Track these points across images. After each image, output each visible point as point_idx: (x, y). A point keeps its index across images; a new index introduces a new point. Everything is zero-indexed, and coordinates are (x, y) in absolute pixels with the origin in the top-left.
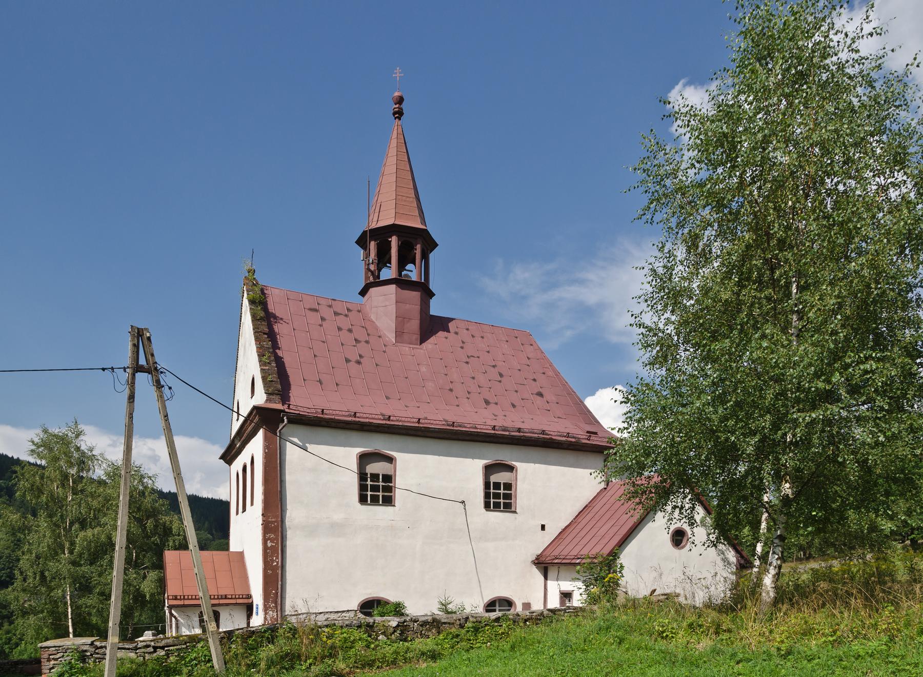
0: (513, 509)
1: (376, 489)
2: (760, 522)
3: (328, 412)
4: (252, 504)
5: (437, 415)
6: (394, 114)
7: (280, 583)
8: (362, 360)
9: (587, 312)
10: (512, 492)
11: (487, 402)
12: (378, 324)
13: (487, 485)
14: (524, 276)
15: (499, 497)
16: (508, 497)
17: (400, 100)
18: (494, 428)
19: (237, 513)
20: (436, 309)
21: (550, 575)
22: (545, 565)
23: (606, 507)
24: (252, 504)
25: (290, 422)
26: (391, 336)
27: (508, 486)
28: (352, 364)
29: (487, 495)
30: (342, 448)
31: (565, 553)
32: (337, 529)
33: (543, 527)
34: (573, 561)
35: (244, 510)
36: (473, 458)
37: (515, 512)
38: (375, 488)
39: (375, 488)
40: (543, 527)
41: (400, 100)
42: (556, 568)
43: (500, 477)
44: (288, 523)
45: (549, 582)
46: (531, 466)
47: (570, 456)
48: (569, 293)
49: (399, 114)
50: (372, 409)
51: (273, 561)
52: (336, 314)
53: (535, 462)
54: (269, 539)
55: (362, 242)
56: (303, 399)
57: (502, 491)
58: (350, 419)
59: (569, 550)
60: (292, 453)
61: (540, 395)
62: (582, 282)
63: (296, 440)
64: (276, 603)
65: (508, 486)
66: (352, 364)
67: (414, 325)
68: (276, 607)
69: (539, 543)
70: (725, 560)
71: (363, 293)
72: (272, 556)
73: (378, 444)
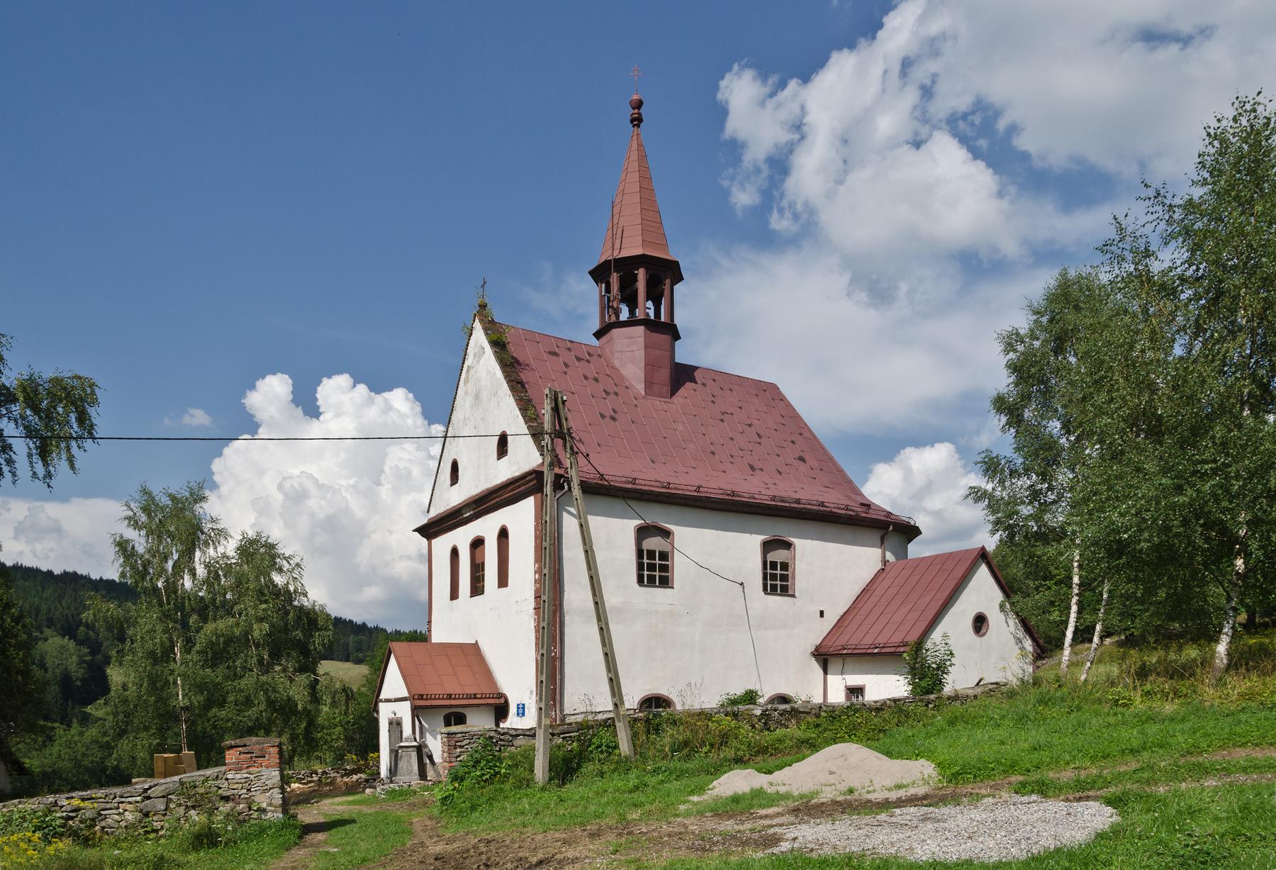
0: (790, 592)
1: (654, 569)
2: (1069, 608)
4: (503, 581)
5: (715, 483)
6: (632, 121)
7: (558, 677)
8: (616, 416)
11: (752, 468)
12: (624, 372)
15: (777, 579)
16: (784, 578)
17: (638, 105)
18: (773, 498)
19: (454, 595)
20: (684, 354)
22: (825, 657)
23: (892, 591)
24: (503, 581)
26: (640, 387)
27: (785, 566)
28: (607, 419)
29: (640, 567)
31: (854, 641)
33: (822, 613)
35: (477, 588)
36: (751, 533)
37: (793, 596)
38: (651, 567)
39: (651, 567)
40: (822, 613)
41: (638, 105)
42: (841, 660)
43: (778, 555)
44: (565, 607)
45: (829, 677)
47: (847, 532)
49: (637, 121)
50: (650, 475)
52: (579, 359)
55: (600, 274)
57: (779, 572)
58: (630, 486)
61: (802, 459)
65: (785, 566)
66: (607, 419)
67: (664, 374)
68: (555, 705)
69: (817, 632)
70: (1022, 649)
71: (598, 335)
73: (781, 529)
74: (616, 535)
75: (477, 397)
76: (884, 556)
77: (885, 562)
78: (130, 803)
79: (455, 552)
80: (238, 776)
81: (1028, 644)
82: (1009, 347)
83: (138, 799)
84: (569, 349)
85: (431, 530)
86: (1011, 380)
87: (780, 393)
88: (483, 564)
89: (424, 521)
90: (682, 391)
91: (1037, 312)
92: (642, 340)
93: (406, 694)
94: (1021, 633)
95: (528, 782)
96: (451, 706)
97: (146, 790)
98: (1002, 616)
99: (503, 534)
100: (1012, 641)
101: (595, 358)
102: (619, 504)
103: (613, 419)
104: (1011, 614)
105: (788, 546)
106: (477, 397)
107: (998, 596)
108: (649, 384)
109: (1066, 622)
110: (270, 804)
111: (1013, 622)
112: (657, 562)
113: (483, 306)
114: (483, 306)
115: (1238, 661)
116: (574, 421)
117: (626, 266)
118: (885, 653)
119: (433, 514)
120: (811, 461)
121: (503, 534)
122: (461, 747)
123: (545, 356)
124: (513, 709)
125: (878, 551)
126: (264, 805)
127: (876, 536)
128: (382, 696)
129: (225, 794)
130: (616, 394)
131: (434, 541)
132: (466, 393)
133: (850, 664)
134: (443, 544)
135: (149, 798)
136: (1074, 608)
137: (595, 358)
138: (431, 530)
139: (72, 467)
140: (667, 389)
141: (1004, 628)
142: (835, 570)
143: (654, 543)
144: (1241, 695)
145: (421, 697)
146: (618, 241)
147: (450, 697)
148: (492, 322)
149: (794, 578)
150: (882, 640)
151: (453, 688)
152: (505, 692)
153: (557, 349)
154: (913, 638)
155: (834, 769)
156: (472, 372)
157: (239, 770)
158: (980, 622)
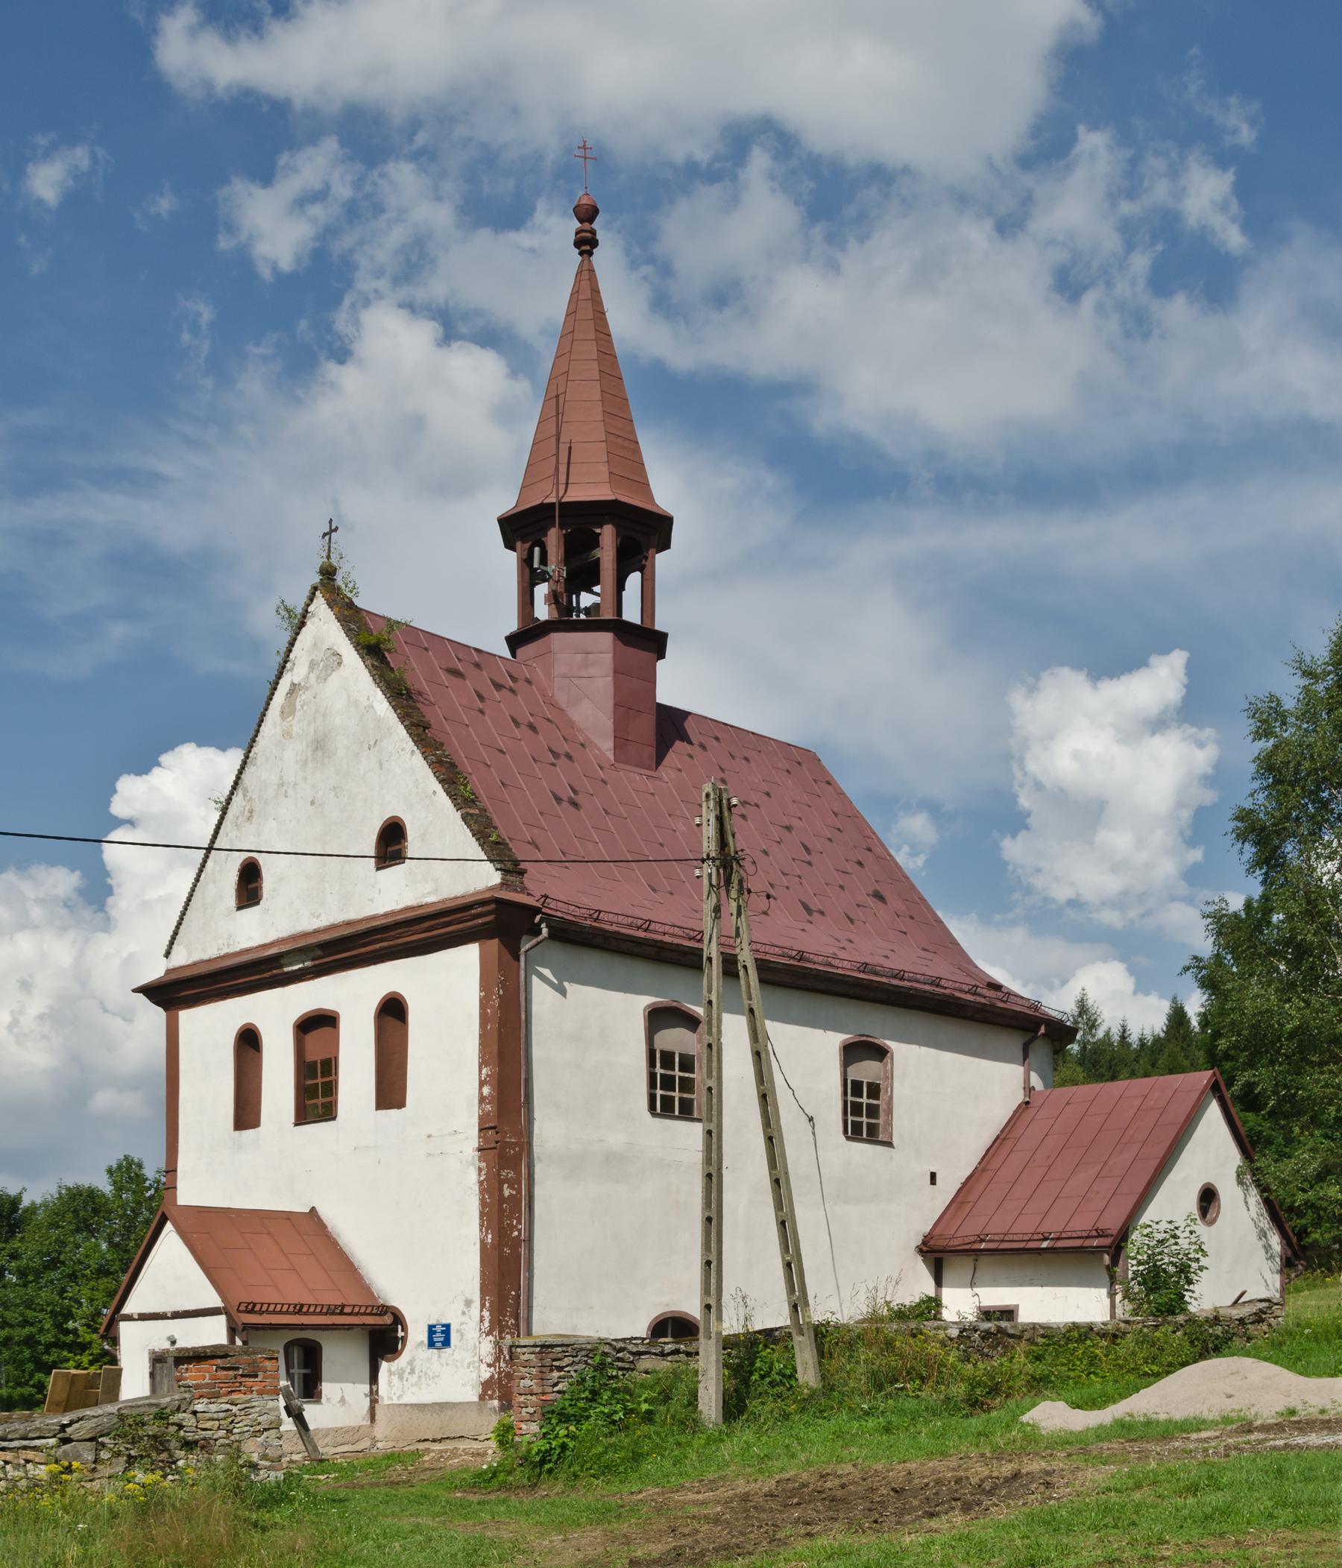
0: (881, 1137)
3: (657, 927)
4: (390, 1091)
8: (578, 799)
13: (651, 1053)
18: (865, 967)
20: (675, 684)
21: (947, 1275)
24: (390, 1091)
25: (552, 936)
26: (606, 746)
27: (874, 1091)
28: (565, 805)
30: (621, 995)
32: (615, 1164)
33: (933, 1177)
34: (976, 1246)
36: (825, 1029)
37: (889, 1144)
38: (668, 1083)
40: (933, 1177)
42: (970, 1259)
43: (866, 1070)
46: (914, 1048)
47: (948, 1028)
51: (512, 1228)
52: (498, 686)
53: (920, 1044)
54: (506, 1181)
57: (864, 1100)
58: (641, 934)
59: (968, 1230)
60: (542, 997)
61: (878, 896)
63: (546, 972)
64: (517, 1317)
67: (646, 726)
68: (517, 1325)
69: (924, 1211)
70: (1267, 1248)
72: (511, 1218)
73: (873, 1023)
74: (592, 1029)
75: (319, 745)
76: (1027, 1080)
77: (1029, 1089)
78: (35, 1448)
79: (248, 1041)
80: (213, 1408)
81: (1275, 1241)
82: (1263, 731)
83: (52, 1441)
84: (477, 665)
85: (174, 993)
87: (823, 769)
88: (336, 1059)
89: (155, 971)
90: (671, 757)
92: (608, 658)
94: (1265, 1223)
95: (689, 1421)
96: (303, 1327)
97: (63, 1427)
98: (1238, 1191)
99: (393, 1010)
100: (1254, 1232)
101: (522, 684)
102: (619, 966)
103: (574, 804)
104: (1254, 1191)
105: (880, 1053)
106: (319, 745)
107: (1232, 1156)
108: (621, 741)
111: (1254, 1197)
112: (677, 1073)
113: (328, 573)
114: (328, 573)
117: (581, 521)
119: (182, 957)
120: (894, 902)
121: (393, 1010)
122: (560, 1369)
123: (444, 677)
124: (416, 1334)
126: (255, 1457)
127: (1014, 1042)
128: (126, 1310)
129: (190, 1437)
130: (569, 757)
131: (186, 1017)
132: (287, 734)
134: (211, 1027)
135: (66, 1441)
137: (522, 684)
138: (174, 993)
140: (650, 751)
141: (1242, 1211)
142: (957, 1098)
145: (251, 1308)
146: (563, 469)
147: (299, 1309)
148: (351, 605)
149: (890, 1112)
150: (1053, 1225)
151: (297, 1294)
152: (394, 1301)
153: (461, 661)
155: (1230, 1392)
156: (303, 697)
157: (214, 1397)
158: (1208, 1197)
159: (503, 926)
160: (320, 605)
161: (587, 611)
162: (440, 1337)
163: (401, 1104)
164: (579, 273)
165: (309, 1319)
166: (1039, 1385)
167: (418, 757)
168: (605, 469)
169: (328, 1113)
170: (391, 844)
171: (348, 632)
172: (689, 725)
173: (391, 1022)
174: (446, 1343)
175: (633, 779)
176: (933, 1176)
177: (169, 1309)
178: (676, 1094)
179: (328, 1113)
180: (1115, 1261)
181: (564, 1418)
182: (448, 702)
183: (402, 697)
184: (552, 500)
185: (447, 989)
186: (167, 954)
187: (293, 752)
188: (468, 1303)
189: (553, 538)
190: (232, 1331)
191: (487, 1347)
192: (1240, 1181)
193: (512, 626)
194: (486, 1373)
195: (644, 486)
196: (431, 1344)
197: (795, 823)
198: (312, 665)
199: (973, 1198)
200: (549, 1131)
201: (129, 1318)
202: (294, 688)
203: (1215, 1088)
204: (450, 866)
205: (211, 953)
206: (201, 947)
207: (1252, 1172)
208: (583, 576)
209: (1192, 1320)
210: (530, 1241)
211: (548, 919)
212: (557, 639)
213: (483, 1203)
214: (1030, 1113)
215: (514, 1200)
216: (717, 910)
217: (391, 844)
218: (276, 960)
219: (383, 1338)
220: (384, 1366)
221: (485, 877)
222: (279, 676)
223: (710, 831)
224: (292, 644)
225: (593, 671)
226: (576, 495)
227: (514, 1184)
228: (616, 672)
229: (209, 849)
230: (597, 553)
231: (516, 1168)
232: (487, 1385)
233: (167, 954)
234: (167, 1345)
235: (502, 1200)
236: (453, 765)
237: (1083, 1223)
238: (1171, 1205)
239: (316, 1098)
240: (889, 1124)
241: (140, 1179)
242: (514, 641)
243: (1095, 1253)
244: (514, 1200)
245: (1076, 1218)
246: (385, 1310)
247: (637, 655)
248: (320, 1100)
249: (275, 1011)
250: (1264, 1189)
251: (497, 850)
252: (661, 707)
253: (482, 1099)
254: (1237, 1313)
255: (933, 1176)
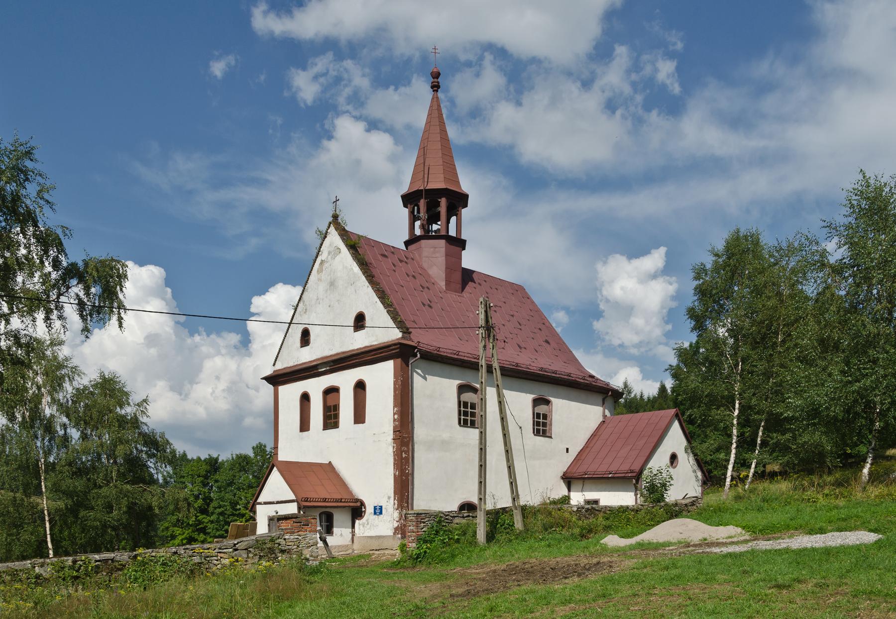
2: (97, 551)
4: (359, 417)
9: (264, 217)
10: (548, 423)
12: (431, 272)
14: (187, 167)
18: (542, 369)
19: (304, 426)
20: (469, 260)
21: (572, 488)
22: (569, 480)
24: (359, 417)
25: (421, 357)
26: (442, 284)
27: (545, 417)
32: (445, 445)
36: (526, 392)
37: (551, 437)
38: (466, 414)
39: (466, 414)
42: (581, 482)
43: (542, 409)
44: (415, 439)
47: (574, 393)
48: (247, 195)
51: (406, 469)
56: (424, 339)
57: (541, 420)
58: (456, 356)
59: (580, 470)
61: (547, 342)
62: (262, 183)
63: (419, 371)
64: (408, 503)
67: (458, 276)
69: (564, 463)
70: (696, 477)
73: (545, 390)
74: (437, 392)
75: (332, 284)
76: (604, 412)
77: (605, 416)
79: (305, 398)
81: (699, 474)
85: (277, 379)
86: (696, 298)
87: (526, 293)
89: (269, 371)
90: (467, 288)
91: (717, 255)
93: (293, 497)
94: (696, 467)
95: (473, 542)
96: (326, 507)
97: (235, 545)
98: (686, 455)
99: (360, 386)
101: (410, 260)
102: (448, 369)
103: (430, 307)
105: (548, 402)
106: (332, 284)
107: (684, 442)
108: (448, 282)
109: (728, 461)
110: (311, 556)
112: (469, 410)
113: (335, 217)
114: (335, 217)
115: (874, 478)
116: (495, 320)
117: (433, 196)
118: (618, 478)
119: (280, 366)
121: (360, 386)
123: (380, 258)
124: (369, 510)
125: (600, 409)
126: (308, 556)
127: (599, 398)
128: (259, 501)
129: (283, 548)
131: (281, 389)
132: (320, 280)
133: (588, 484)
134: (290, 393)
135: (236, 550)
136: (734, 451)
137: (410, 260)
138: (277, 379)
139: (121, 326)
141: (686, 463)
142: (576, 419)
143: (468, 397)
144: (876, 496)
146: (426, 176)
147: (325, 500)
149: (551, 425)
150: (613, 468)
153: (387, 251)
154: (636, 468)
156: (326, 265)
157: (292, 533)
158: (674, 458)
159: (402, 354)
160: (332, 229)
161: (435, 231)
162: (378, 511)
163: (363, 422)
164: (433, 98)
165: (328, 503)
166: (608, 529)
167: (370, 288)
168: (442, 176)
169: (336, 425)
170: (360, 322)
171: (343, 240)
172: (474, 276)
173: (360, 390)
174: (381, 513)
175: (452, 296)
176: (567, 449)
177: (275, 500)
178: (469, 418)
179: (336, 425)
180: (637, 482)
181: (425, 542)
182: (381, 267)
183: (364, 265)
184: (422, 188)
185: (381, 377)
186: (274, 365)
187: (322, 287)
188: (389, 498)
189: (422, 203)
190: (299, 508)
191: (396, 514)
192: (686, 452)
193: (407, 238)
194: (396, 524)
195: (457, 183)
196: (375, 513)
197: (515, 313)
198: (329, 253)
199: (583, 458)
200: (420, 432)
201: (260, 504)
202: (322, 262)
203: (677, 415)
204: (383, 330)
205: (291, 364)
206: (288, 362)
207: (691, 448)
208: (434, 217)
209: (667, 504)
210: (413, 474)
211: (420, 350)
212: (424, 242)
213: (395, 459)
214: (605, 425)
215: (407, 459)
216: (485, 347)
217: (360, 322)
218: (315, 367)
219: (357, 511)
220: (357, 522)
221: (396, 334)
222: (317, 257)
223: (482, 316)
224: (321, 245)
225: (437, 255)
226: (431, 186)
227: (407, 452)
228: (447, 255)
229: (290, 323)
230: (439, 209)
231: (408, 446)
232: (396, 529)
233: (274, 365)
234: (274, 514)
235: (402, 458)
236: (383, 291)
237: (625, 467)
238: (659, 461)
239: (331, 420)
240: (551, 429)
241: (264, 451)
242: (407, 243)
243: (629, 479)
244: (407, 459)
245: (622, 466)
246: (357, 500)
247: (454, 248)
248: (333, 421)
249: (315, 387)
250: (695, 455)
251: (400, 324)
252: (463, 269)
253: (394, 420)
254: (684, 502)
255: (567, 449)
